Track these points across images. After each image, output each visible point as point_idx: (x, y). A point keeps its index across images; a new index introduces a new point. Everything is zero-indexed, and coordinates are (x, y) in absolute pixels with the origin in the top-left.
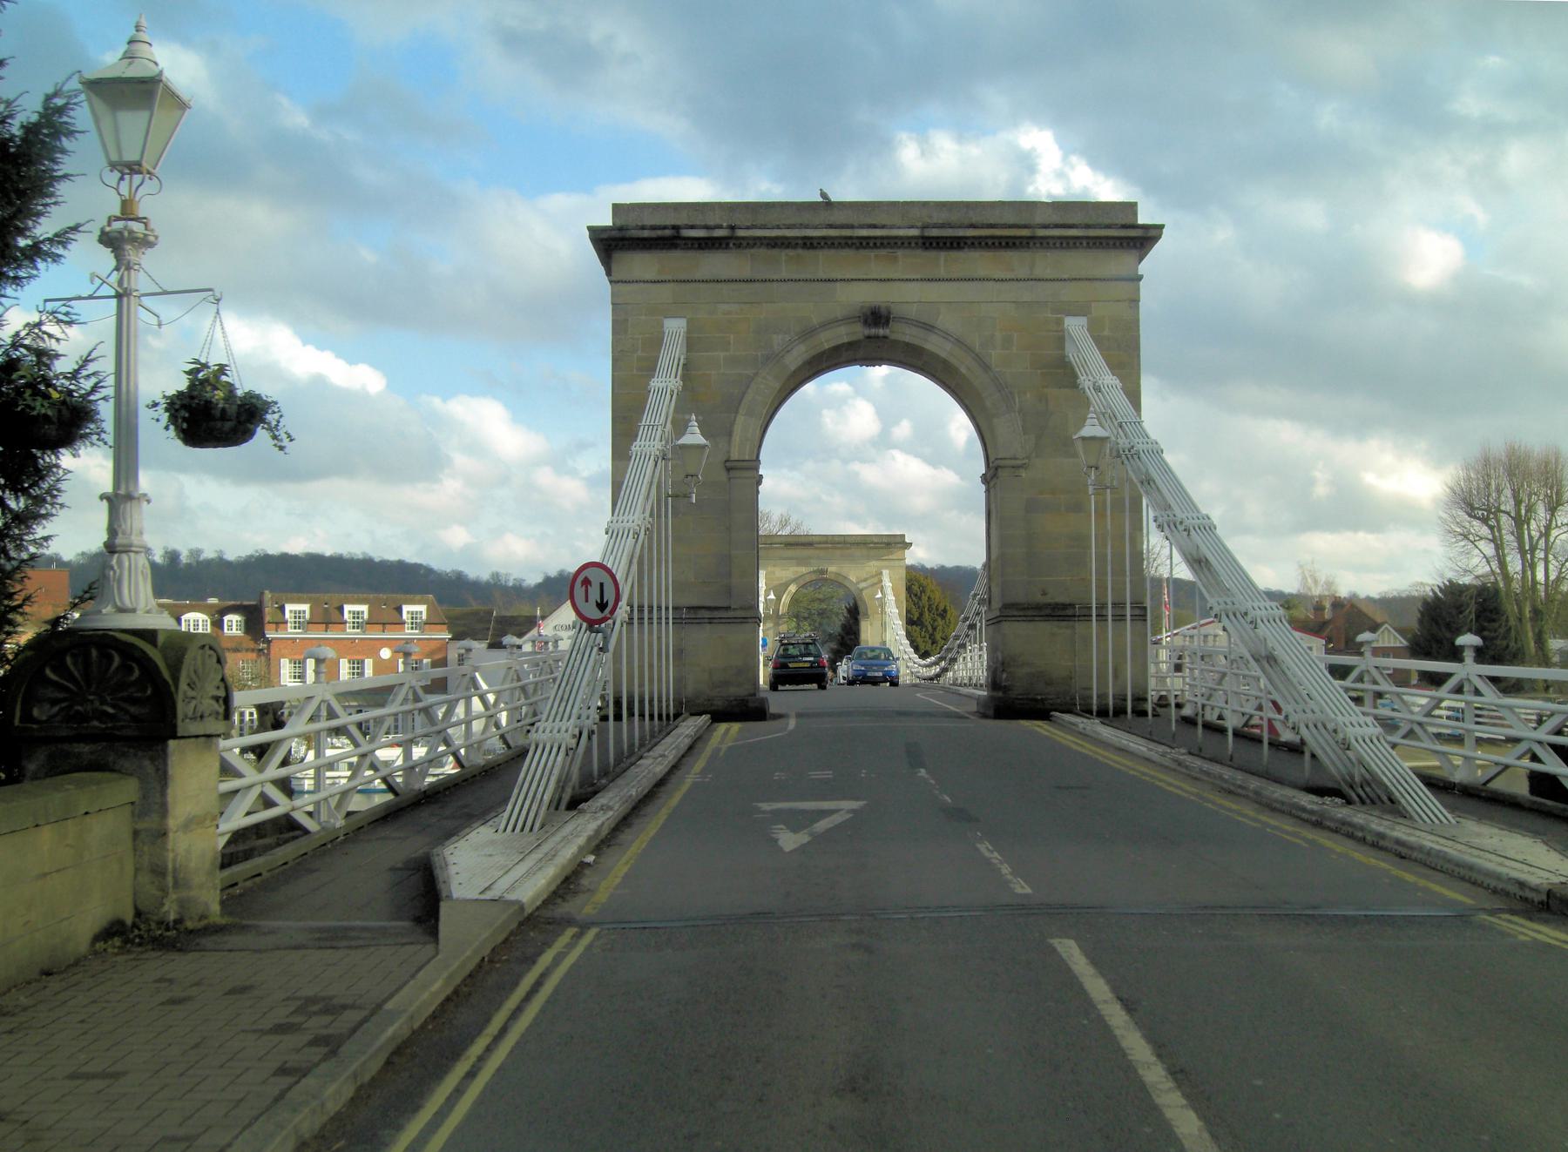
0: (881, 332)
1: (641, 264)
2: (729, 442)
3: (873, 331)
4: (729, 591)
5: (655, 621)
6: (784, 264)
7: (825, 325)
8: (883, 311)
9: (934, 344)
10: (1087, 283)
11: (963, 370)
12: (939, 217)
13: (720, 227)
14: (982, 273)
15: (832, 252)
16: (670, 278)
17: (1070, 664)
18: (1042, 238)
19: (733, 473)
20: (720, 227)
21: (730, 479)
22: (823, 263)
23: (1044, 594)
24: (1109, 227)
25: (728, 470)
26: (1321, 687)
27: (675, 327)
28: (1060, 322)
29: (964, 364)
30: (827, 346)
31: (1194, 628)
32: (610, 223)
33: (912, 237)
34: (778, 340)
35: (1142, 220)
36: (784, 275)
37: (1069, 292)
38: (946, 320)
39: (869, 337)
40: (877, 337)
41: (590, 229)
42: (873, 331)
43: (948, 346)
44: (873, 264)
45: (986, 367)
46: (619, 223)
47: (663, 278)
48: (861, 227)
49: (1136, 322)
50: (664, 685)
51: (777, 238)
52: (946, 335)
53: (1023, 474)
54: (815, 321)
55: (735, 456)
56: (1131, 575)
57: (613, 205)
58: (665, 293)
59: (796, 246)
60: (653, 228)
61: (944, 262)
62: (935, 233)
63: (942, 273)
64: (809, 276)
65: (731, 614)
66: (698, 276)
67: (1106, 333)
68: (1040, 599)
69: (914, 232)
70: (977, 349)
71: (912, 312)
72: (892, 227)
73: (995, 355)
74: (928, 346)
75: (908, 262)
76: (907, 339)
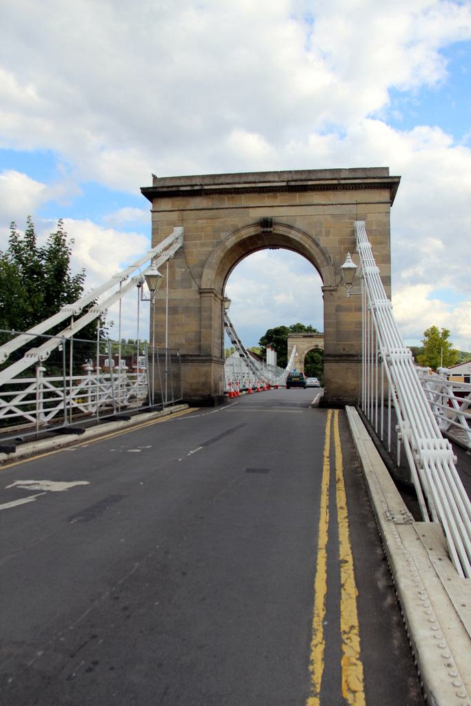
0: (269, 229)
1: (166, 204)
2: (200, 281)
3: (265, 229)
4: (200, 348)
5: (372, 355)
6: (227, 202)
7: (243, 228)
8: (269, 220)
9: (293, 235)
10: (364, 205)
11: (307, 246)
12: (296, 177)
13: (197, 185)
14: (315, 202)
15: (248, 195)
16: (177, 209)
17: (355, 383)
18: (343, 184)
19: (202, 295)
20: (197, 185)
21: (201, 297)
22: (244, 200)
23: (344, 350)
24: (374, 178)
25: (200, 293)
26: (408, 397)
27: (178, 231)
28: (352, 223)
29: (308, 244)
30: (245, 237)
31: (107, 380)
32: (152, 186)
33: (283, 186)
34: (223, 235)
35: (391, 174)
36: (226, 206)
37: (361, 209)
38: (299, 224)
39: (263, 232)
40: (267, 232)
41: (141, 189)
42: (265, 229)
43: (300, 235)
44: (267, 200)
45: (317, 245)
46: (155, 186)
47: (174, 209)
48: (260, 182)
49: (389, 222)
50: (377, 401)
51: (222, 189)
52: (299, 230)
53: (334, 293)
54: (240, 226)
55: (203, 287)
56: (62, 364)
57: (388, 168)
58: (175, 216)
59: (231, 193)
60: (168, 187)
61: (298, 198)
62: (293, 183)
63: (297, 202)
64: (238, 206)
65: (200, 358)
66: (189, 208)
67: (374, 228)
68: (342, 352)
69: (284, 184)
70: (314, 237)
71: (284, 220)
72: (274, 182)
73: (323, 242)
74: (291, 236)
75: (280, 199)
76: (281, 233)
